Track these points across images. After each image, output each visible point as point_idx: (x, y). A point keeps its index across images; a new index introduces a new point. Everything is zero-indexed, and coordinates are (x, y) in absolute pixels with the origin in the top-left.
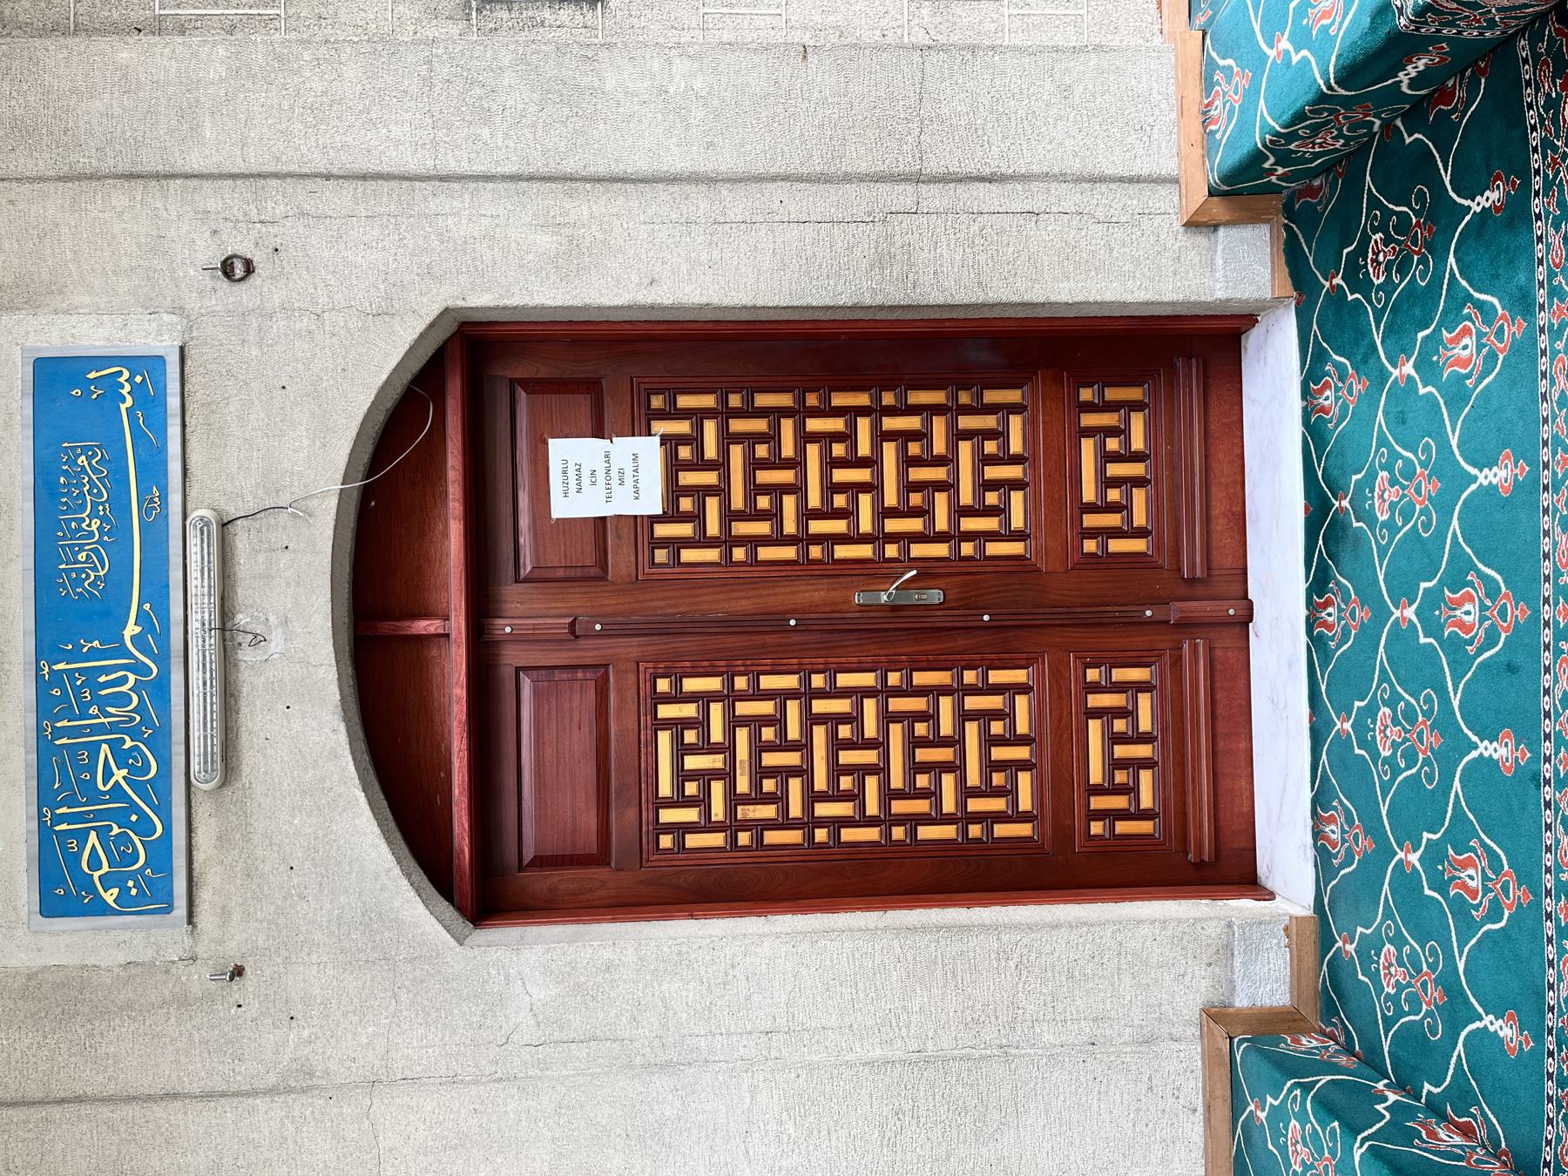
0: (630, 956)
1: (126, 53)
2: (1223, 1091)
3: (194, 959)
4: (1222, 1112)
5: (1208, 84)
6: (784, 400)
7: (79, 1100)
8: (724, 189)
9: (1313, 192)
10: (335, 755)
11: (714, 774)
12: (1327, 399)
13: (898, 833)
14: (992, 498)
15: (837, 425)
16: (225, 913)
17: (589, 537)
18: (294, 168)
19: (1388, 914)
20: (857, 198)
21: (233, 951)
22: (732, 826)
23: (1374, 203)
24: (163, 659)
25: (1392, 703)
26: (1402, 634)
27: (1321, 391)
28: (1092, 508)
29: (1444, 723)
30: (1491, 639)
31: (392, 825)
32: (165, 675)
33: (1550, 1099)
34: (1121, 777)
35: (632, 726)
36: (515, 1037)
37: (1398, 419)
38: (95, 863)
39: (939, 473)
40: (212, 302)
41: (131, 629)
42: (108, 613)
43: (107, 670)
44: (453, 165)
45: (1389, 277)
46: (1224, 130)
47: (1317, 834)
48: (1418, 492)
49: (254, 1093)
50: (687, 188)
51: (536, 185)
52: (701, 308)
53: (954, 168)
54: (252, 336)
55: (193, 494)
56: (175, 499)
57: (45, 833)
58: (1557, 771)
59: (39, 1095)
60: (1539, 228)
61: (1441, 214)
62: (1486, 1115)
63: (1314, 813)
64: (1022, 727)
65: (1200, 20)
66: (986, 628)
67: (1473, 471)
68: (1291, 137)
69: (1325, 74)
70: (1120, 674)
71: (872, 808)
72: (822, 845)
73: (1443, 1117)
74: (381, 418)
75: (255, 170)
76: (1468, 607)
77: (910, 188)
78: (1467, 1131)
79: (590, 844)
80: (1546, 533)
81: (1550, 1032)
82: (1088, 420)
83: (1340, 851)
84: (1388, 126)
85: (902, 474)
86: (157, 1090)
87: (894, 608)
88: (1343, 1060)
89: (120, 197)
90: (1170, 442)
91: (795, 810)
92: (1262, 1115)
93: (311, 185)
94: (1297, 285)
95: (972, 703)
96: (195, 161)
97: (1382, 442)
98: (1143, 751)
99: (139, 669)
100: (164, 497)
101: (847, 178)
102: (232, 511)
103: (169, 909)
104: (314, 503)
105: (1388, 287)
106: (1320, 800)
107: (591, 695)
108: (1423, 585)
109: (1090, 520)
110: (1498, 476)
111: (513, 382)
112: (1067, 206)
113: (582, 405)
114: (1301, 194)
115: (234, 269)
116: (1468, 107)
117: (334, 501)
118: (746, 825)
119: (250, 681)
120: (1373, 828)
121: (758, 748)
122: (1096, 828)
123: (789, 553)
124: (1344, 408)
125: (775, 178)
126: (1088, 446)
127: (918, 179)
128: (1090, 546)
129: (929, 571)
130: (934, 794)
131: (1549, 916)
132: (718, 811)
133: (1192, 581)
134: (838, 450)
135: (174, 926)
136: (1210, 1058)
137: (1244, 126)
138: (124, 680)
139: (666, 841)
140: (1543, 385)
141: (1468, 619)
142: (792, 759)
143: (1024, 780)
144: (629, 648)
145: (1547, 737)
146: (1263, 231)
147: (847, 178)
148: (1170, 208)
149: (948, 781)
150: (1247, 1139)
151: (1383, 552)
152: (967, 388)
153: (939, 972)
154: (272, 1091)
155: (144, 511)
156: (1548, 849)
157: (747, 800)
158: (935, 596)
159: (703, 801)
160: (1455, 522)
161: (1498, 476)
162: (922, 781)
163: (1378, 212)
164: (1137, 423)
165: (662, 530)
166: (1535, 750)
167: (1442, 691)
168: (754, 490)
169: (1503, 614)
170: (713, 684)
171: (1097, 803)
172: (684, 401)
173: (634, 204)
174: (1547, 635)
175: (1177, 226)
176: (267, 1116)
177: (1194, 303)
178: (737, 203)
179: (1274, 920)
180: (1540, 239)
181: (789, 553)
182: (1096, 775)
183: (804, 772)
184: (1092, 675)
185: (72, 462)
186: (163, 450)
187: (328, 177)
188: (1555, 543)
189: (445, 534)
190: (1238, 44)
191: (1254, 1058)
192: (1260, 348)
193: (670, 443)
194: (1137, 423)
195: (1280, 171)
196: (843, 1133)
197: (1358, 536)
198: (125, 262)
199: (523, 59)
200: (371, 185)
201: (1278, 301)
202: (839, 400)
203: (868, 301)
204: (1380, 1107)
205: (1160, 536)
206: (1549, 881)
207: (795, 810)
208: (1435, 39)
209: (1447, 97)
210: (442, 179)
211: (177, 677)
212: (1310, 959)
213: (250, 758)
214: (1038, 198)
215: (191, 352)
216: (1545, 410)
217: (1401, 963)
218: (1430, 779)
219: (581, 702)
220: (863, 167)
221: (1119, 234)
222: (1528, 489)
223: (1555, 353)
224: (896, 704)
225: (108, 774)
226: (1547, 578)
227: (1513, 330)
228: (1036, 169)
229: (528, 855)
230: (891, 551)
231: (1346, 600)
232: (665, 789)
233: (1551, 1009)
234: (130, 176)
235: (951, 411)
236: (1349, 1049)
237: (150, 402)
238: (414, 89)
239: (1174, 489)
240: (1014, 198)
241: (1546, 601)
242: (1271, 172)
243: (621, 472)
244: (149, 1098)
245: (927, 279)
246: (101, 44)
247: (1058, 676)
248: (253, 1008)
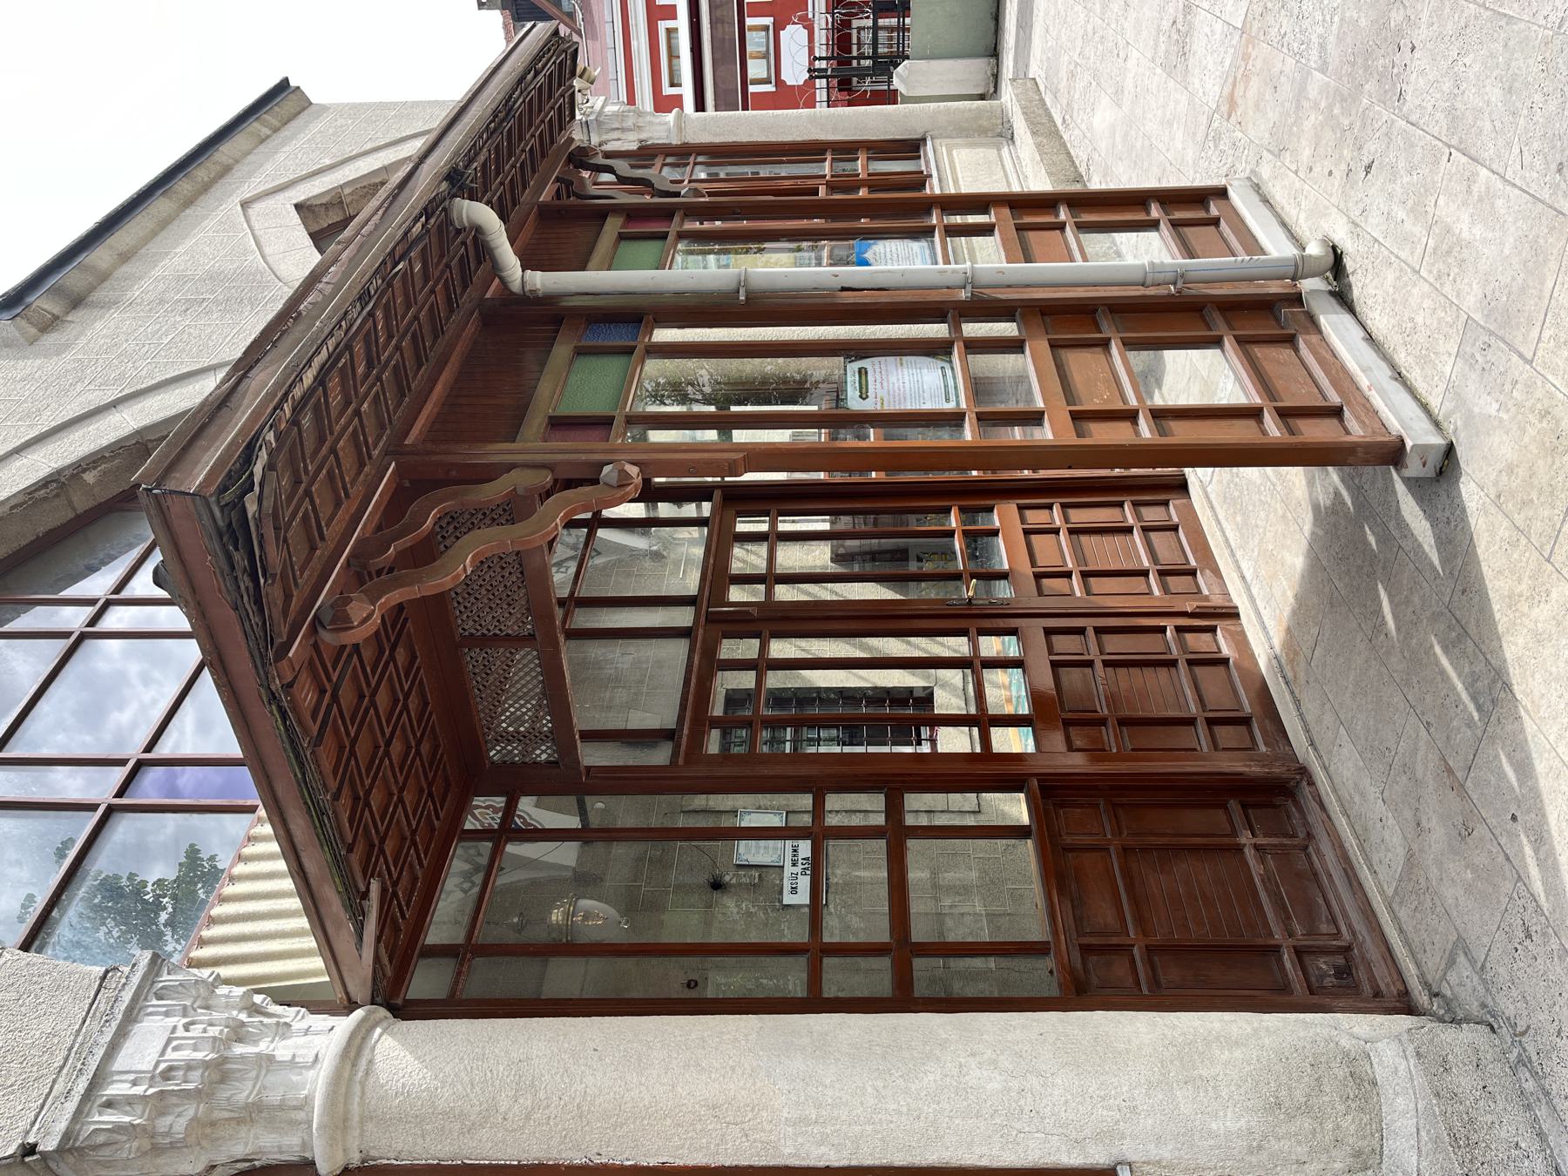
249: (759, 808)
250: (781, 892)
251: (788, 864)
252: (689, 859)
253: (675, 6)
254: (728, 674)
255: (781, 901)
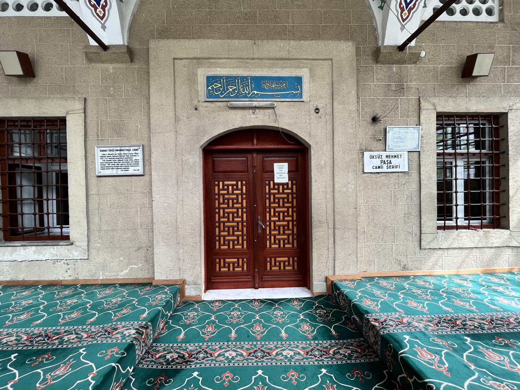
0: (197, 176)
1: (354, 92)
2: (171, 283)
3: (199, 102)
4: (167, 283)
5: (351, 280)
6: (295, 204)
7: (175, 82)
8: (332, 194)
9: (333, 300)
10: (233, 126)
11: (228, 192)
12: (295, 303)
13: (217, 224)
14: (277, 241)
15: (290, 214)
16: (206, 107)
17: (270, 170)
18: (334, 120)
19: (202, 314)
20: (331, 218)
21: (200, 108)
22: (219, 194)
23: (331, 311)
24: (251, 97)
25: (241, 314)
26: (254, 316)
27: (297, 302)
28: (275, 260)
29: (238, 324)
30: (254, 333)
31: (221, 135)
32: (248, 98)
33: (169, 345)
34: (227, 265)
35: (237, 177)
36: (183, 156)
37: (293, 315)
38: (216, 86)
39: (282, 232)
40: (311, 106)
41: (256, 92)
42: (259, 88)
43: (249, 88)
44: (335, 147)
45: (318, 314)
46: (344, 283)
47: (216, 301)
48: (280, 319)
49: (175, 111)
50: (332, 188)
51: (332, 161)
52: (311, 190)
53: (336, 235)
54: (306, 113)
55: (279, 103)
56: (278, 100)
57: (221, 77)
58: (230, 345)
59: (175, 75)
60: (329, 342)
61: (330, 323)
62: (166, 332)
63: (220, 300)
64: (236, 247)
65: (362, 279)
66: (254, 240)
67: (284, 329)
68: (343, 295)
69: (355, 301)
70: (245, 265)
71: (222, 220)
72: (215, 211)
73: (165, 324)
74: (292, 134)
75: (334, 114)
76: (259, 328)
77: (332, 227)
78: (163, 329)
79: (217, 169)
80: (273, 343)
81: (182, 345)
82: (291, 259)
83: (214, 305)
84: (346, 313)
85: (281, 225)
86: (176, 95)
87: (258, 224)
88: (176, 305)
89: (329, 92)
90: (287, 274)
91: (221, 206)
92: (166, 290)
93: (332, 123)
94: (316, 297)
95: (240, 238)
96: (335, 104)
97: (288, 313)
98: (231, 269)
99: (249, 93)
100: (278, 98)
101: (334, 216)
102: (276, 109)
103: (207, 98)
104: (277, 123)
105: (316, 313)
106: (223, 301)
107: (243, 170)
108: (263, 320)
109: (273, 259)
110: (283, 334)
111: (297, 157)
112: (330, 255)
113: (294, 169)
114: (332, 297)
115: (317, 110)
116: (350, 328)
117: (277, 126)
118: (219, 197)
119: (246, 112)
120: (218, 311)
121: (233, 199)
122: (218, 260)
123: (268, 205)
124: (294, 306)
125: (334, 203)
126: (286, 259)
127: (334, 228)
128: (268, 259)
129: (264, 230)
130: (224, 231)
131: (203, 344)
132: (222, 192)
133: (262, 278)
134: (286, 214)
135: (205, 98)
136: (176, 281)
137: (345, 287)
138: (247, 91)
139: (216, 183)
140: (300, 342)
141: (257, 328)
142: (231, 205)
143: (226, 247)
144: (251, 177)
145: (236, 343)
146: (325, 291)
147: (334, 216)
148: (329, 273)
149: (226, 233)
150: (161, 287)
151: (269, 313)
152: (297, 237)
153: (193, 231)
154: (175, 115)
155: (276, 95)
156: (215, 344)
157: (223, 197)
158: (260, 231)
159: (223, 189)
160: (274, 326)
161: (283, 334)
162: (226, 229)
163: (125, 355)
164: (290, 268)
165: (272, 182)
166: (234, 341)
167: (243, 324)
168: (279, 199)
169: (258, 335)
170: (244, 191)
171: (222, 261)
172: (294, 187)
173: (329, 178)
174: (255, 343)
175: (326, 275)
176: (171, 114)
177: (312, 278)
178: (329, 196)
179: (201, 293)
180: (327, 342)
181: (268, 205)
182: (227, 260)
183: (228, 207)
184: (245, 260)
185: (284, 83)
186: (286, 98)
187: (333, 126)
188: (271, 345)
189: (271, 145)
190: (359, 286)
191: (176, 289)
192: (304, 291)
193: (287, 184)
194: (290, 268)
195: (336, 294)
196: (164, 214)
197: (271, 308)
198: (318, 92)
199: (354, 159)
200: (332, 133)
201: (313, 294)
202: (295, 214)
203: (312, 219)
204: (167, 312)
205: (270, 272)
206: (210, 344)
207: (221, 206)
208: (363, 322)
209: (352, 324)
210: (333, 145)
211: (247, 100)
212: (194, 299)
213: (233, 112)
214: (331, 250)
215: (303, 103)
216: (296, 342)
217: (193, 316)
218: (228, 321)
219: (241, 168)
220: (336, 219)
221: (325, 264)
222: (281, 339)
223: (306, 344)
224: (240, 224)
225: (231, 88)
226: (265, 343)
227: (310, 336)
228: (336, 249)
229: (215, 159)
230: (268, 223)
231: (259, 306)
232: (226, 183)
233: (186, 345)
234: (333, 93)
235: (293, 234)
236: (177, 306)
237: (295, 96)
238: (348, 141)
239: (278, 275)
240: (331, 246)
241: (261, 343)
242: (336, 292)
243: (282, 175)
244: (175, 94)
245: (317, 230)
246: (355, 88)
247: (245, 254)
248: (190, 112)
249: (422, 137)
250: (371, 151)
251: (387, 153)
252: (390, 104)
253: (505, 115)
254: (494, 21)
255: (366, 150)
